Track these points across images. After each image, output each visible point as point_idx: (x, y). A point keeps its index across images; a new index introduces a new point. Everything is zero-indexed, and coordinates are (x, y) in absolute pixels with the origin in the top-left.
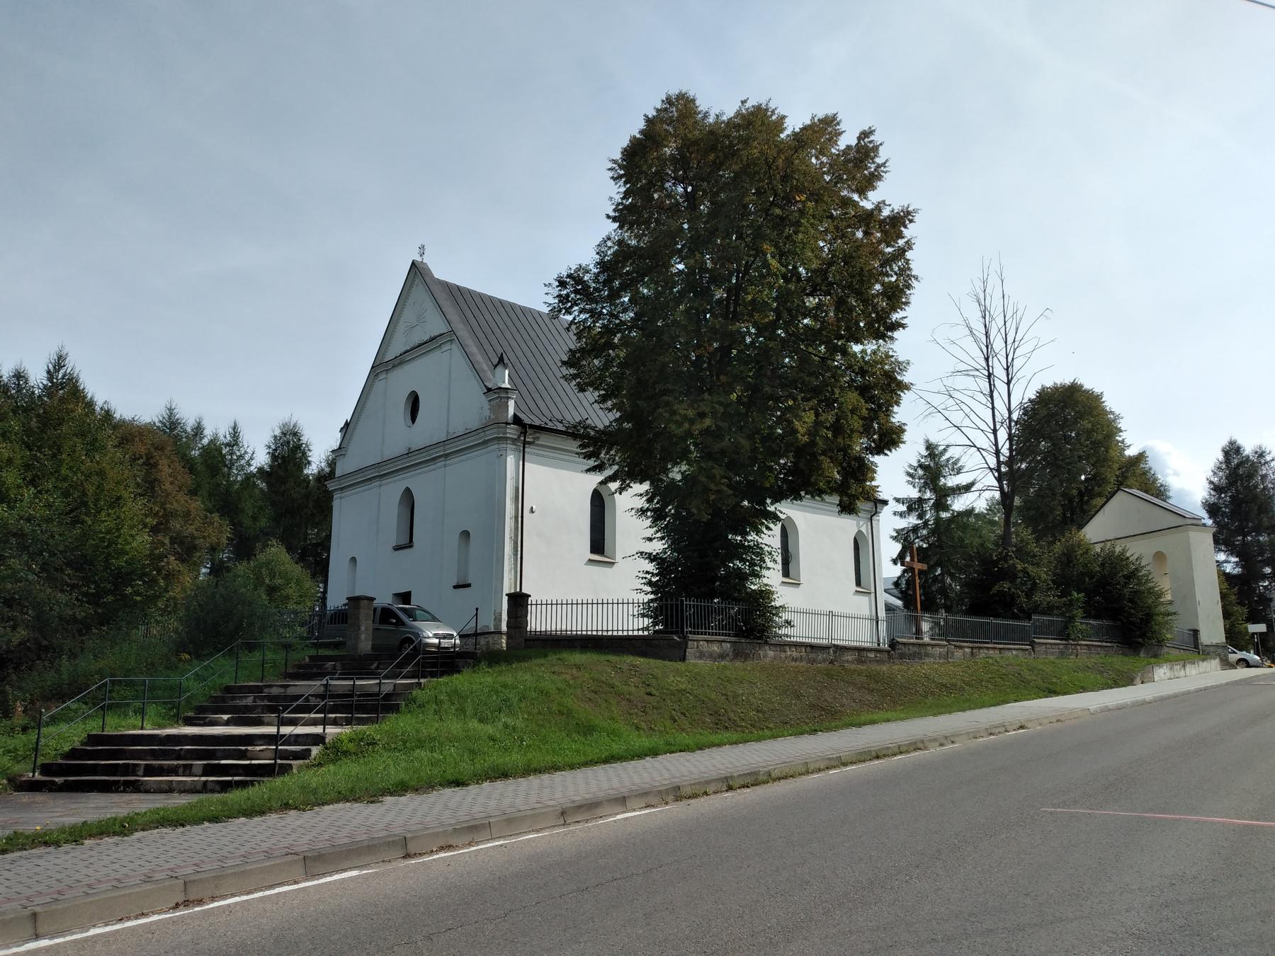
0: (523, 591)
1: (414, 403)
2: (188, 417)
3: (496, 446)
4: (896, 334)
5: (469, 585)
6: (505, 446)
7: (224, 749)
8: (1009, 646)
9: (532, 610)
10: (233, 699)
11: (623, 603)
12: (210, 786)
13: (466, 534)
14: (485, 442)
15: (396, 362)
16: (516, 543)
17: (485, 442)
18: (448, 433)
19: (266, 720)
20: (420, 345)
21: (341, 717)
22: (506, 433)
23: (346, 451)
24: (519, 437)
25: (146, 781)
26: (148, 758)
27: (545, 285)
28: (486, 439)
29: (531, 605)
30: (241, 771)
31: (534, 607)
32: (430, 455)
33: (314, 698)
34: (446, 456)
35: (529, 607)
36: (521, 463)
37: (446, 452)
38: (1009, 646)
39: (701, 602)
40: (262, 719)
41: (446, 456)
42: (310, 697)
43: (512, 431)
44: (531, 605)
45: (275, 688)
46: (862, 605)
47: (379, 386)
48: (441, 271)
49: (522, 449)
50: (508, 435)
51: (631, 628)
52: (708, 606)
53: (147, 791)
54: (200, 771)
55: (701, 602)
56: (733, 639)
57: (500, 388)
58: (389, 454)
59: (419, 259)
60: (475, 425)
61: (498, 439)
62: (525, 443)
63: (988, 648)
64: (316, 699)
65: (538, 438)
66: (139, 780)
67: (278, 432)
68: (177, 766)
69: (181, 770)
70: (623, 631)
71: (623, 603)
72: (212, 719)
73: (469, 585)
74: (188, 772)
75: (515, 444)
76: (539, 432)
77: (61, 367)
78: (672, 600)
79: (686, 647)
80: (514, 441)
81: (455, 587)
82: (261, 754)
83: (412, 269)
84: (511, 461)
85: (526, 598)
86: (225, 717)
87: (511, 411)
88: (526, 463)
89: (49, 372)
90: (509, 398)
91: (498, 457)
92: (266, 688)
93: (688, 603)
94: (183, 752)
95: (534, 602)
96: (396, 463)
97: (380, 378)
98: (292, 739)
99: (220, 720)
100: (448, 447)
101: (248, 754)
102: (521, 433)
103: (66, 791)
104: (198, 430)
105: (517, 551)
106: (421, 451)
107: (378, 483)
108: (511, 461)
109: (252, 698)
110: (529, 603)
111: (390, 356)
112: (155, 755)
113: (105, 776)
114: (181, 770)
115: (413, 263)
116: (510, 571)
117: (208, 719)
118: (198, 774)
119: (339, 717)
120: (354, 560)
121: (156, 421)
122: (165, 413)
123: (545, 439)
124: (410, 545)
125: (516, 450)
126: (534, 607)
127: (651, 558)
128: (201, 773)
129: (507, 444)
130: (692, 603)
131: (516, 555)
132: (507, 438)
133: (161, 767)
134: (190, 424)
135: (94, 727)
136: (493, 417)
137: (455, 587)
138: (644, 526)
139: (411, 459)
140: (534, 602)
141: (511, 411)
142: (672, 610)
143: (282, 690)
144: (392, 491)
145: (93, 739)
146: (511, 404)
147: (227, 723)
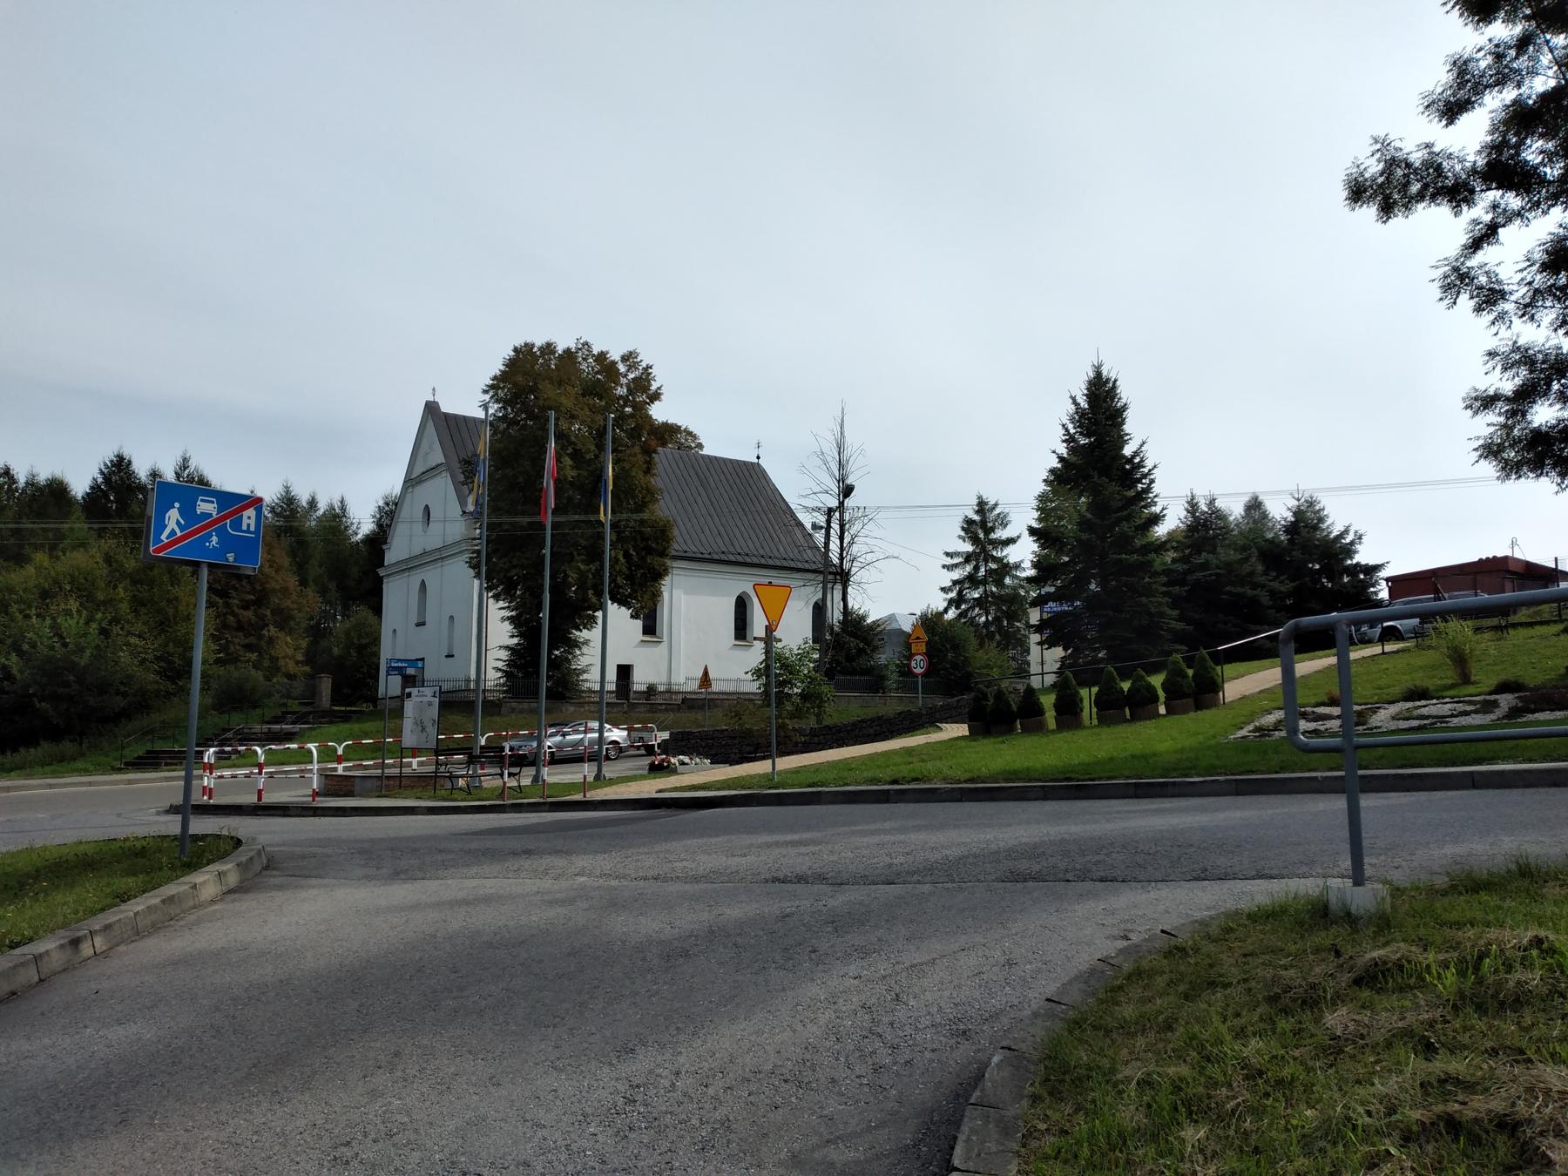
0: (1559, 568)
2: (303, 495)
4: (1105, 373)
15: (418, 480)
34: (442, 558)
46: (682, 680)
60: (458, 538)
67: (381, 503)
77: (185, 468)
89: (176, 473)
104: (313, 503)
112: (171, 758)
120: (395, 630)
121: (275, 498)
122: (282, 491)
124: (424, 624)
127: (507, 648)
134: (304, 500)
135: (149, 747)
138: (508, 627)
144: (415, 579)
145: (148, 752)
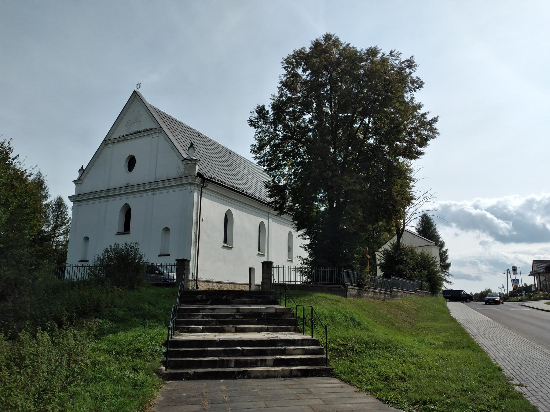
1: (131, 163)
3: (189, 187)
5: (169, 255)
6: (193, 187)
7: (272, 349)
8: (411, 292)
9: (274, 271)
10: (190, 316)
11: (286, 268)
12: (294, 373)
13: (167, 230)
14: (182, 184)
15: (121, 139)
16: (196, 235)
17: (182, 184)
18: (155, 178)
19: (226, 329)
20: (131, 134)
21: (271, 328)
22: (195, 181)
23: (83, 182)
24: (200, 183)
25: (252, 371)
26: (222, 355)
27: (251, 112)
28: (183, 183)
29: (274, 268)
30: (297, 363)
31: (275, 269)
32: (144, 188)
33: (239, 316)
35: (273, 268)
36: (200, 197)
37: (155, 188)
38: (411, 292)
39: (325, 268)
40: (224, 328)
41: (154, 189)
42: (236, 315)
43: (198, 180)
44: (274, 268)
45: (207, 310)
47: (109, 149)
48: (150, 99)
49: (200, 190)
50: (196, 182)
51: (297, 281)
52: (332, 271)
53: (250, 377)
54: (271, 363)
55: (325, 268)
56: (357, 288)
57: (192, 159)
58: (113, 185)
59: (137, 90)
61: (191, 183)
62: (202, 187)
63: (411, 294)
64: (240, 316)
65: (207, 185)
66: (247, 371)
68: (257, 361)
69: (259, 363)
70: (283, 281)
71: (286, 268)
72: (193, 329)
73: (169, 255)
74: (264, 364)
75: (198, 187)
76: (208, 182)
78: (323, 268)
79: (347, 291)
80: (198, 185)
81: (159, 256)
82: (295, 352)
83: (134, 93)
84: (196, 194)
85: (186, 262)
86: (201, 327)
87: (197, 171)
88: (202, 198)
90: (196, 164)
91: (190, 192)
92: (201, 310)
93: (321, 269)
94: (245, 351)
95: (275, 267)
96: (120, 191)
97: (108, 146)
98: (300, 342)
99: (198, 329)
100: (157, 185)
101: (287, 352)
102: (202, 182)
103: (198, 379)
105: (197, 239)
106: (139, 186)
107: (106, 199)
108: (196, 194)
109: (201, 316)
110: (176, 267)
111: (116, 135)
113: (209, 367)
114: (259, 363)
115: (135, 91)
116: (194, 249)
117: (191, 329)
118: (270, 365)
119: (270, 327)
120: (87, 239)
123: (210, 186)
125: (198, 190)
126: (275, 269)
128: (272, 365)
129: (194, 186)
130: (321, 269)
131: (196, 241)
132: (195, 184)
133: (246, 361)
136: (186, 172)
137: (159, 256)
139: (131, 189)
140: (275, 267)
141: (197, 171)
142: (327, 273)
143: (211, 311)
146: (197, 167)
147: (203, 331)
